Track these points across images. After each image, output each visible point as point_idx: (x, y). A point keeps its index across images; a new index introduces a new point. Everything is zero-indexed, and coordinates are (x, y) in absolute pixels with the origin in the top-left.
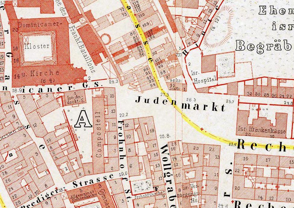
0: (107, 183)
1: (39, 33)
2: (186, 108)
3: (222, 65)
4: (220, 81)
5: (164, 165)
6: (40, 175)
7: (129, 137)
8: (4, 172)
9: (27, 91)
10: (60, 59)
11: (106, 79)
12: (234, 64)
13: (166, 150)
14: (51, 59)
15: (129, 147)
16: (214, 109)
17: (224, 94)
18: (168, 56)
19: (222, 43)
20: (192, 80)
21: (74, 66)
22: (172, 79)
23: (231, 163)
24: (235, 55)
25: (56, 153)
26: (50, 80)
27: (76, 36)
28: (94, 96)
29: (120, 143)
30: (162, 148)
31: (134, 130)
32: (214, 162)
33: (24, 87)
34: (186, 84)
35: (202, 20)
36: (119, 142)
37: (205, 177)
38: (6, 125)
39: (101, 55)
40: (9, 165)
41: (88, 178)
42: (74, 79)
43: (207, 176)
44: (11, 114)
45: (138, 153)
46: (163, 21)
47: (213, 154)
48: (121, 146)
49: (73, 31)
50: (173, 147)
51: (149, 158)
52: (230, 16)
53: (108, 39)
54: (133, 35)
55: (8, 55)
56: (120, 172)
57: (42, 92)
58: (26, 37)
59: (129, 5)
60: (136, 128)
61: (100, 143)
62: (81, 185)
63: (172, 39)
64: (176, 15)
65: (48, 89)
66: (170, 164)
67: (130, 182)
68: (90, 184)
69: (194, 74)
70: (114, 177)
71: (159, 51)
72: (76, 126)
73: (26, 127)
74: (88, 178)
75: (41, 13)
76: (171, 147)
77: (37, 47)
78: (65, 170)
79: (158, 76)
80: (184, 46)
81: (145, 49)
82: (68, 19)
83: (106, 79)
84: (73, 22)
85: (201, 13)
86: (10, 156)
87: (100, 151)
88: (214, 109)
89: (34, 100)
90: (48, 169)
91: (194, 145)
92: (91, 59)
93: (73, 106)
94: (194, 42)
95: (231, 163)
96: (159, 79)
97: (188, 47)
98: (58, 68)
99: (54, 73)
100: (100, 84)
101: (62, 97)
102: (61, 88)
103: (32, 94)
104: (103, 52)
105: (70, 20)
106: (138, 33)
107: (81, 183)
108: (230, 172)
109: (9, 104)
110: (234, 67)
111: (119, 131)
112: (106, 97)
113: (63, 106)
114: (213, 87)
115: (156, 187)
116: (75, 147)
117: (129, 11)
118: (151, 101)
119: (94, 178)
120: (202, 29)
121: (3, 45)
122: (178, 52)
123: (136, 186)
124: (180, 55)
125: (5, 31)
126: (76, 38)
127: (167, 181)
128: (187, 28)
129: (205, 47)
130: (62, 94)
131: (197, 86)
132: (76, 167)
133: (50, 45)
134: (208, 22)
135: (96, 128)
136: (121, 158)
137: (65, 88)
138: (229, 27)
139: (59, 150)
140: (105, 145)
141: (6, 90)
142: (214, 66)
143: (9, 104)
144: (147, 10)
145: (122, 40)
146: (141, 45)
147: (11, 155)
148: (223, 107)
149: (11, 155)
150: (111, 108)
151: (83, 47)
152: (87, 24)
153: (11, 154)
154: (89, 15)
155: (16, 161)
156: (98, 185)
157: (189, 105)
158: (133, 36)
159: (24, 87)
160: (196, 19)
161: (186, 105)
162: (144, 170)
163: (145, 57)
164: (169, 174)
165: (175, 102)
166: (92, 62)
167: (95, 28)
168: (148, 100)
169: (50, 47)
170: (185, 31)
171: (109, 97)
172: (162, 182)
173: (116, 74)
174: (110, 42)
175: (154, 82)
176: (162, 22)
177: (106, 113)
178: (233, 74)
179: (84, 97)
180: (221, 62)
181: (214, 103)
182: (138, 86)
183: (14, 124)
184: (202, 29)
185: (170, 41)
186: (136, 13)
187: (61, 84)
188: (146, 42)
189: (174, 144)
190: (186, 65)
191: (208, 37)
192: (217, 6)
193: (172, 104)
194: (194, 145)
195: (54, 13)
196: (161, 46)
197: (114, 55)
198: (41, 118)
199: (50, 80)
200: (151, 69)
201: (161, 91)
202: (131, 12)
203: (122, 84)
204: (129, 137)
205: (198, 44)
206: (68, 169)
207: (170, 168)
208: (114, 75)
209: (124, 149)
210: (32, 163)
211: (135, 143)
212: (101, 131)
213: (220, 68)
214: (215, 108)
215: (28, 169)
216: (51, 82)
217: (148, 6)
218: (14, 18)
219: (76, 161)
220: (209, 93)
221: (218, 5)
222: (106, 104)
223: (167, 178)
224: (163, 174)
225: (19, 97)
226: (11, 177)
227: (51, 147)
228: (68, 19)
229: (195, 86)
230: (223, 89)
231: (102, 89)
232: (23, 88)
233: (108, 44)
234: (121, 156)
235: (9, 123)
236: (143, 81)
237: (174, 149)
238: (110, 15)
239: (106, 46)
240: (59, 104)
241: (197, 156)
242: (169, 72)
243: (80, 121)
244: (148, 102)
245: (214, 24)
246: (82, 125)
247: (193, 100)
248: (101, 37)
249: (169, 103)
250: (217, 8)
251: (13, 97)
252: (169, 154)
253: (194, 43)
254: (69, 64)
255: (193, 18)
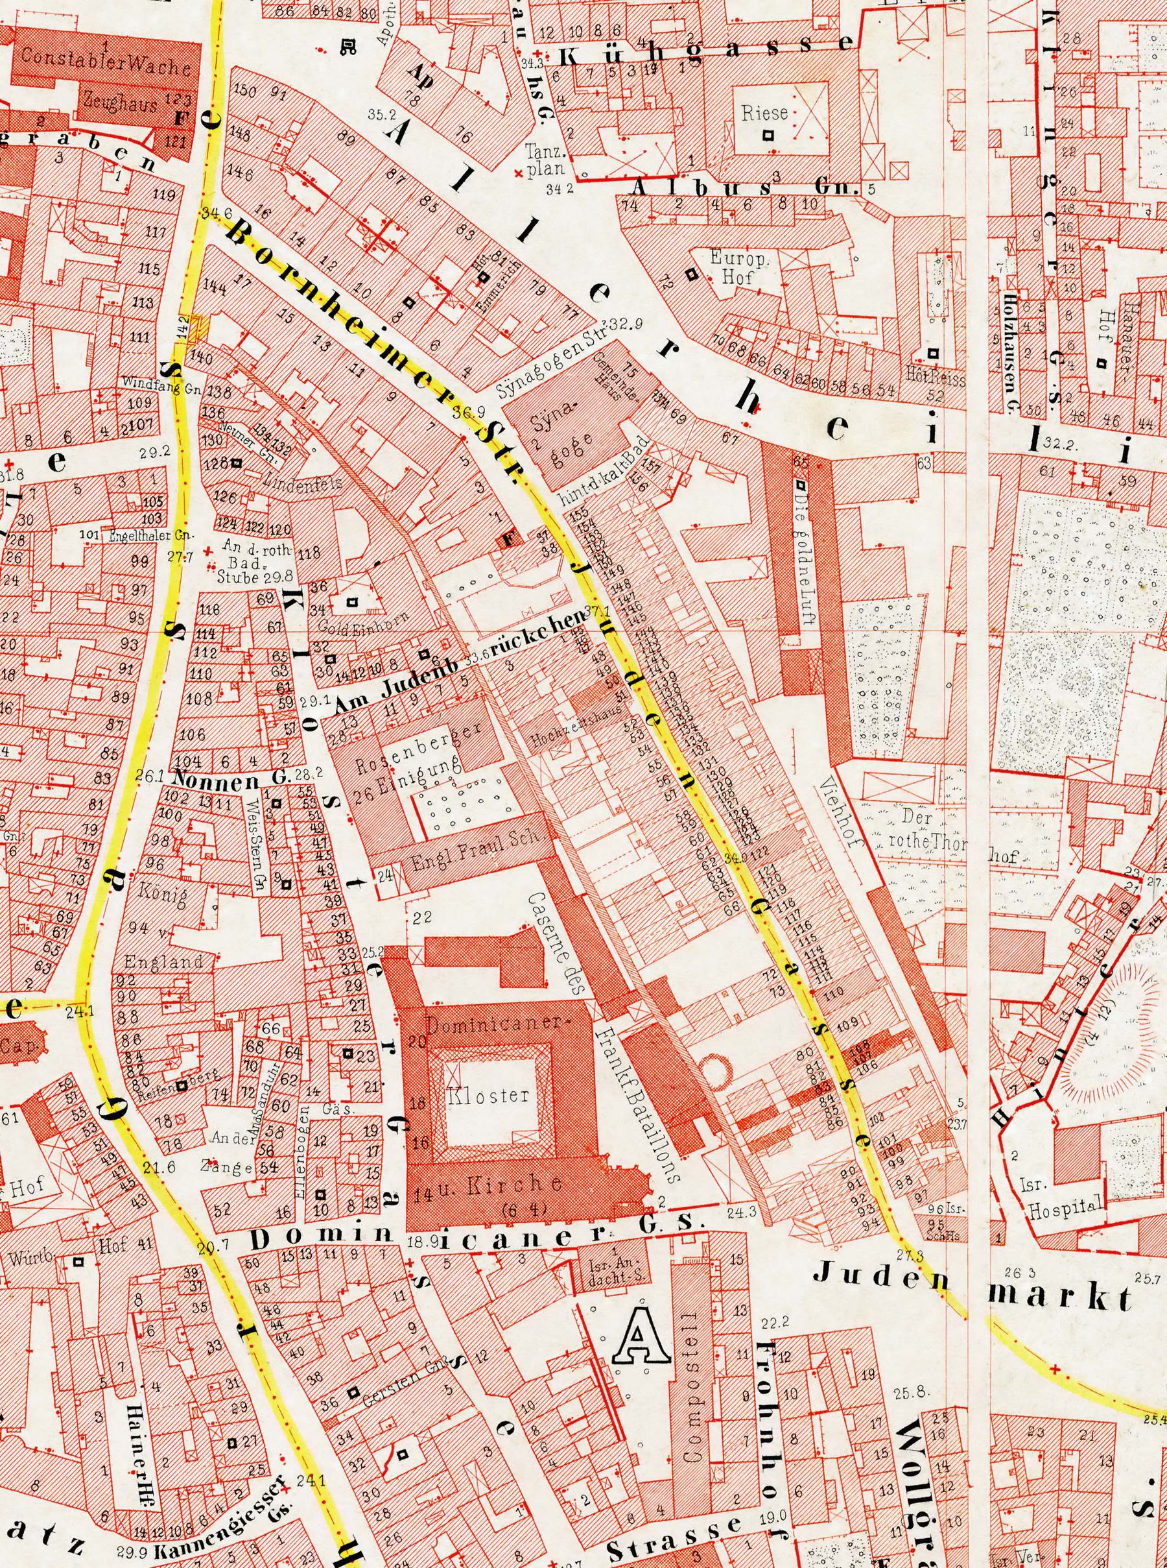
0: (719, 1546)
1: (495, 1053)
2: (1002, 1300)
3: (1119, 1157)
4: (1116, 1212)
5: (909, 1489)
6: (498, 1522)
7: (791, 1394)
8: (380, 1509)
9: (455, 1244)
10: (565, 1139)
11: (717, 1204)
12: (1162, 1157)
13: (915, 1439)
14: (536, 1137)
15: (792, 1427)
16: (1096, 1302)
17: (1129, 1254)
18: (920, 1129)
19: (1120, 1085)
20: (1023, 1208)
21: (613, 1162)
22: (936, 1205)
23: (1152, 1482)
24: (1163, 1125)
25: (551, 1449)
26: (534, 1208)
27: (617, 1063)
28: (679, 1261)
29: (762, 1415)
30: (902, 1432)
31: (810, 1372)
32: (1094, 1476)
33: (446, 1230)
34: (1004, 1220)
35: (1055, 1010)
36: (759, 1412)
37: (1064, 1528)
38: (387, 1355)
39: (701, 1124)
40: (395, 1487)
41: (657, 1531)
42: (610, 1203)
43: (1071, 1522)
44: (403, 1320)
45: (821, 1450)
46: (904, 1011)
47: (1092, 1451)
48: (765, 1424)
49: (607, 1046)
50: (936, 1428)
51: (860, 1465)
52: (1150, 996)
53: (724, 1071)
54: (807, 1060)
55: (393, 1124)
56: (762, 1510)
57: (504, 1245)
58: (452, 1065)
59: (794, 959)
60: (815, 1365)
61: (697, 1417)
62: (635, 1555)
63: (932, 1072)
64: (946, 994)
65: (527, 1236)
66: (927, 1486)
67: (796, 1542)
68: (664, 1552)
69: (1029, 1187)
70: (743, 1528)
71: (892, 1112)
72: (617, 1359)
73: (454, 1364)
74: (657, 1531)
75: (502, 987)
76: (931, 1427)
77: (488, 1099)
78: (580, 1503)
79: (888, 1192)
80: (998, 1095)
81: (845, 1107)
82: (592, 1005)
83: (717, 1204)
84: (608, 1017)
85: (1053, 987)
86: (400, 1459)
87: (697, 1441)
88: (1096, 1302)
89: (478, 1272)
90: (525, 1503)
91: (1031, 1422)
92: (667, 1136)
93: (609, 1292)
94: (1029, 1081)
95: (1152, 1482)
96: (892, 1203)
97: (1008, 1098)
98: (558, 1169)
99: (545, 1182)
100: (698, 1219)
101: (571, 1265)
102: (568, 1235)
103: (472, 1254)
104: (709, 1116)
105: (598, 1008)
106: (822, 1052)
107: (632, 1549)
108: (1149, 1511)
109: (396, 1287)
110: (1162, 1165)
111: (761, 1376)
112: (717, 1263)
113: (575, 1294)
114: (1090, 1232)
115: (881, 1562)
116: (615, 1428)
117: (791, 980)
118: (866, 1278)
119: (677, 1530)
120: (1057, 1039)
121: (375, 1091)
122: (952, 1113)
123: (815, 1559)
124: (962, 1124)
125: (384, 1046)
126: (617, 1070)
127: (918, 1542)
128: (1007, 1038)
129: (1067, 1099)
130: (572, 1255)
131: (1040, 1228)
132: (616, 1494)
133: (533, 1091)
134: (1076, 1017)
135: (682, 1368)
136: (765, 1466)
137: (581, 1232)
138: (1144, 1032)
139: (562, 1439)
140: (714, 1420)
141: (388, 1239)
142: (1095, 1163)
143: (396, 1287)
144: (852, 978)
145: (768, 1075)
146: (833, 1093)
147: (402, 1455)
148: (1124, 1296)
149: (403, 1455)
150: (732, 1300)
151: (640, 1097)
152: (653, 1021)
153: (404, 1451)
154: (660, 990)
155: (421, 1474)
156: (688, 1552)
157: (1013, 1290)
158: (807, 1060)
159: (446, 1230)
160: (1034, 1006)
161: (1003, 1289)
162: (841, 1505)
163: (845, 1131)
164: (923, 1519)
165: (945, 1279)
166: (671, 1148)
167: (680, 1034)
168: (856, 1272)
169: (532, 1098)
170: (1000, 1046)
171: (726, 1264)
172: (900, 1544)
173: (749, 1190)
174: (729, 1082)
175: (877, 1215)
176: (902, 1017)
177: (718, 1316)
178: (1159, 1188)
179: (644, 1267)
180: (1120, 1150)
181: (1094, 1284)
182: (823, 1228)
183: (415, 1353)
184: (1057, 1039)
185: (929, 1078)
186: (816, 986)
187: (569, 1222)
188: (849, 1081)
189: (941, 1419)
190: (1002, 1157)
191: (1073, 1068)
192: (1105, 966)
193: (935, 1286)
194: (1031, 1422)
195: (545, 985)
196: (899, 1095)
197: (743, 1125)
198: (503, 1333)
199: (534, 1208)
200: (867, 1173)
201: (900, 1246)
202: (799, 983)
203: (769, 1222)
204: (791, 1394)
205: (1043, 1088)
206: (592, 1502)
207: (929, 1499)
208: (741, 1191)
209: (776, 1435)
210: (474, 1481)
211: (811, 1414)
212: (698, 1377)
213: (1114, 1168)
214: (1099, 1301)
215: (460, 1498)
216: (535, 1213)
217: (856, 963)
218: (412, 1001)
219: (617, 1473)
220: (1079, 1250)
221: (1109, 960)
222: (716, 1285)
223: (918, 1532)
224: (906, 1518)
225: (428, 1261)
226: (402, 1529)
227: (535, 1430)
228: (593, 1007)
229: (1031, 1228)
230: (1126, 1238)
231: (704, 1237)
232: (442, 1233)
233: (721, 1088)
234: (765, 1458)
235: (398, 1348)
236: (838, 1211)
237: (942, 1434)
238: (730, 991)
239: (716, 1094)
240: (563, 1287)
241: (1040, 1457)
242: (924, 1181)
243: (629, 1343)
244: (855, 1281)
245: (1094, 1024)
246: (639, 1355)
247: (1025, 1273)
248: (701, 1064)
249: (926, 1282)
250: (1106, 971)
251: (410, 1264)
252: (923, 1451)
253: (1028, 1087)
254: (594, 1156)
255: (1026, 1006)
